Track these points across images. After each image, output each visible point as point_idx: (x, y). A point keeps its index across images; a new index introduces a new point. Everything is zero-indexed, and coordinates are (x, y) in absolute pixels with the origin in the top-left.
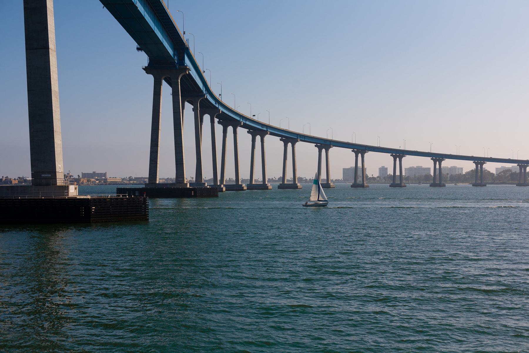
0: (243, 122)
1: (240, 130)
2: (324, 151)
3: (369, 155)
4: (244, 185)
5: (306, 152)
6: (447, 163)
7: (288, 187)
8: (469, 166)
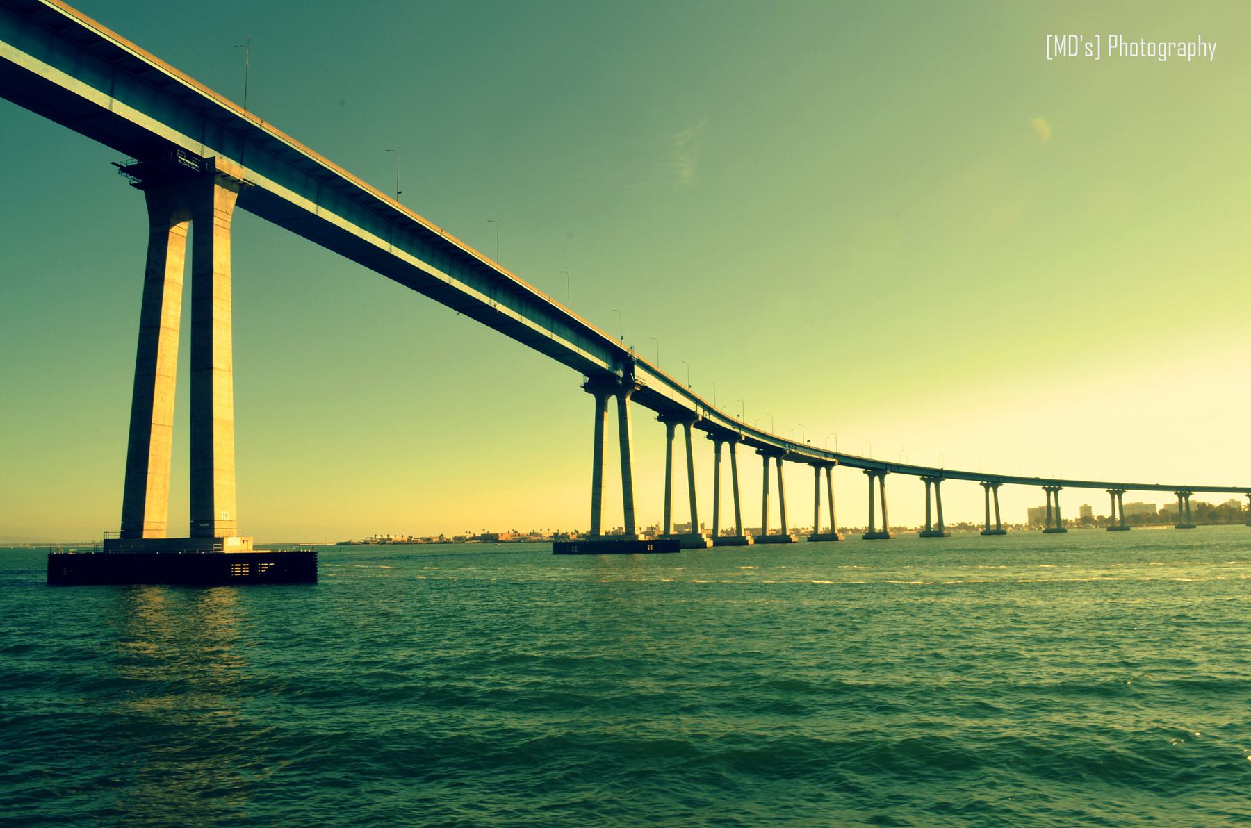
0: (744, 434)
1: (739, 446)
2: (877, 479)
3: (1065, 492)
4: (748, 538)
5: (849, 481)
6: (1130, 497)
7: (823, 539)
8: (1171, 498)
